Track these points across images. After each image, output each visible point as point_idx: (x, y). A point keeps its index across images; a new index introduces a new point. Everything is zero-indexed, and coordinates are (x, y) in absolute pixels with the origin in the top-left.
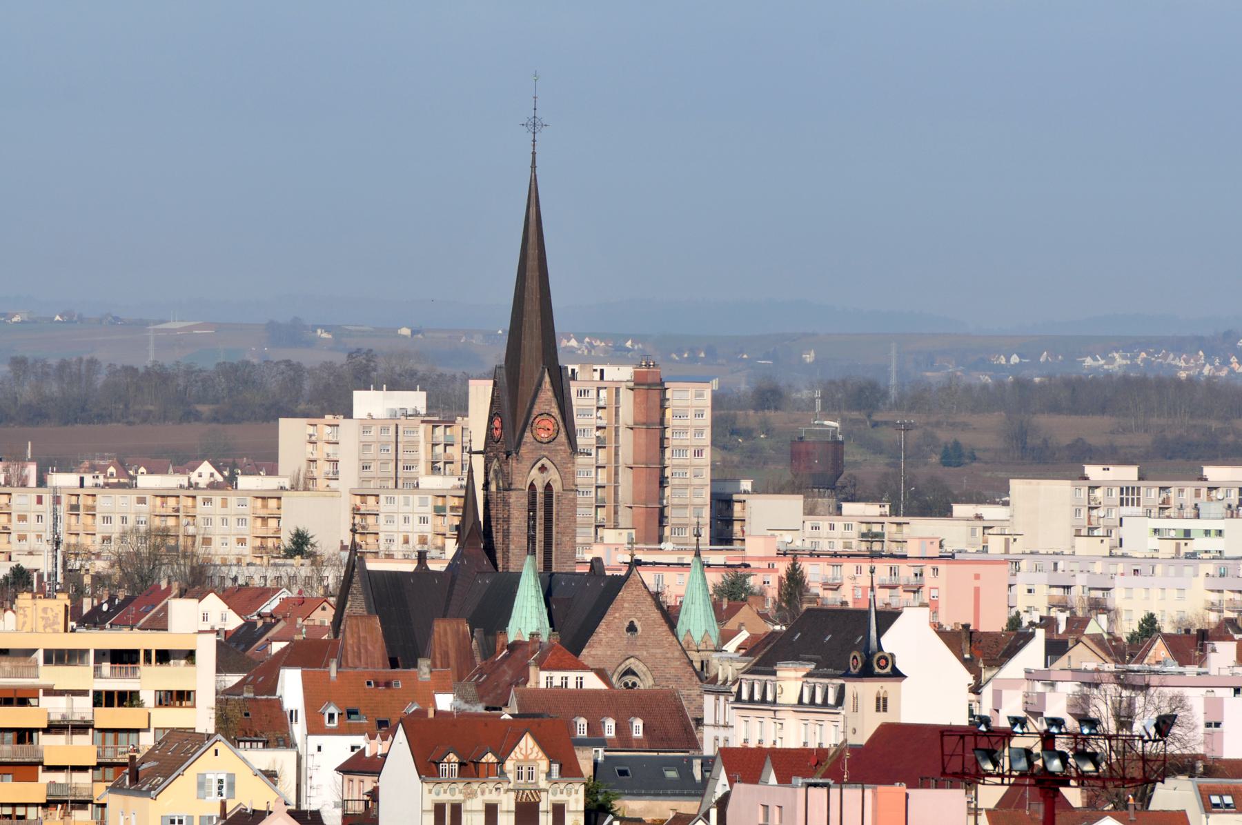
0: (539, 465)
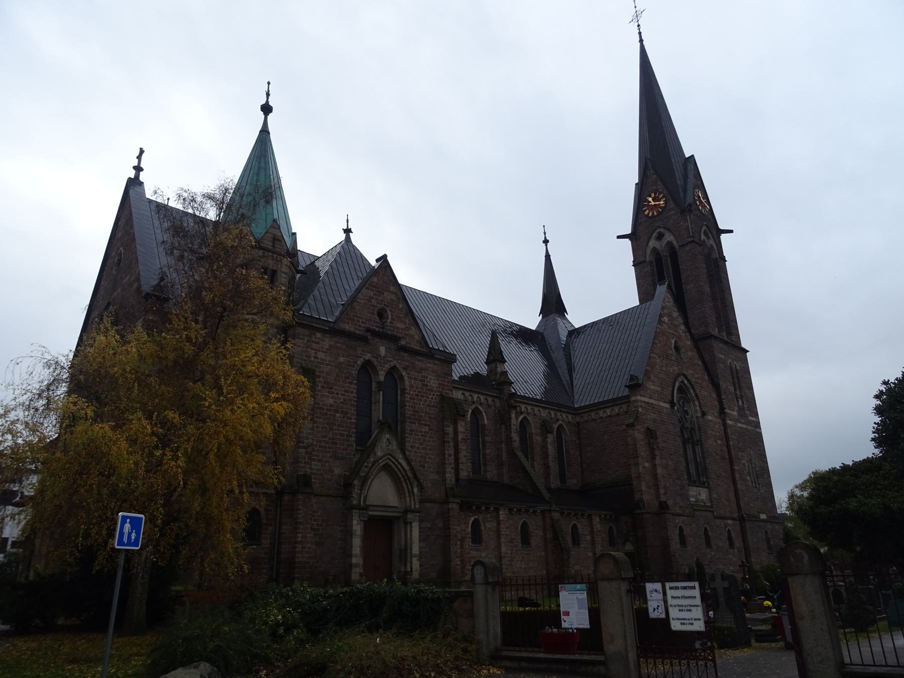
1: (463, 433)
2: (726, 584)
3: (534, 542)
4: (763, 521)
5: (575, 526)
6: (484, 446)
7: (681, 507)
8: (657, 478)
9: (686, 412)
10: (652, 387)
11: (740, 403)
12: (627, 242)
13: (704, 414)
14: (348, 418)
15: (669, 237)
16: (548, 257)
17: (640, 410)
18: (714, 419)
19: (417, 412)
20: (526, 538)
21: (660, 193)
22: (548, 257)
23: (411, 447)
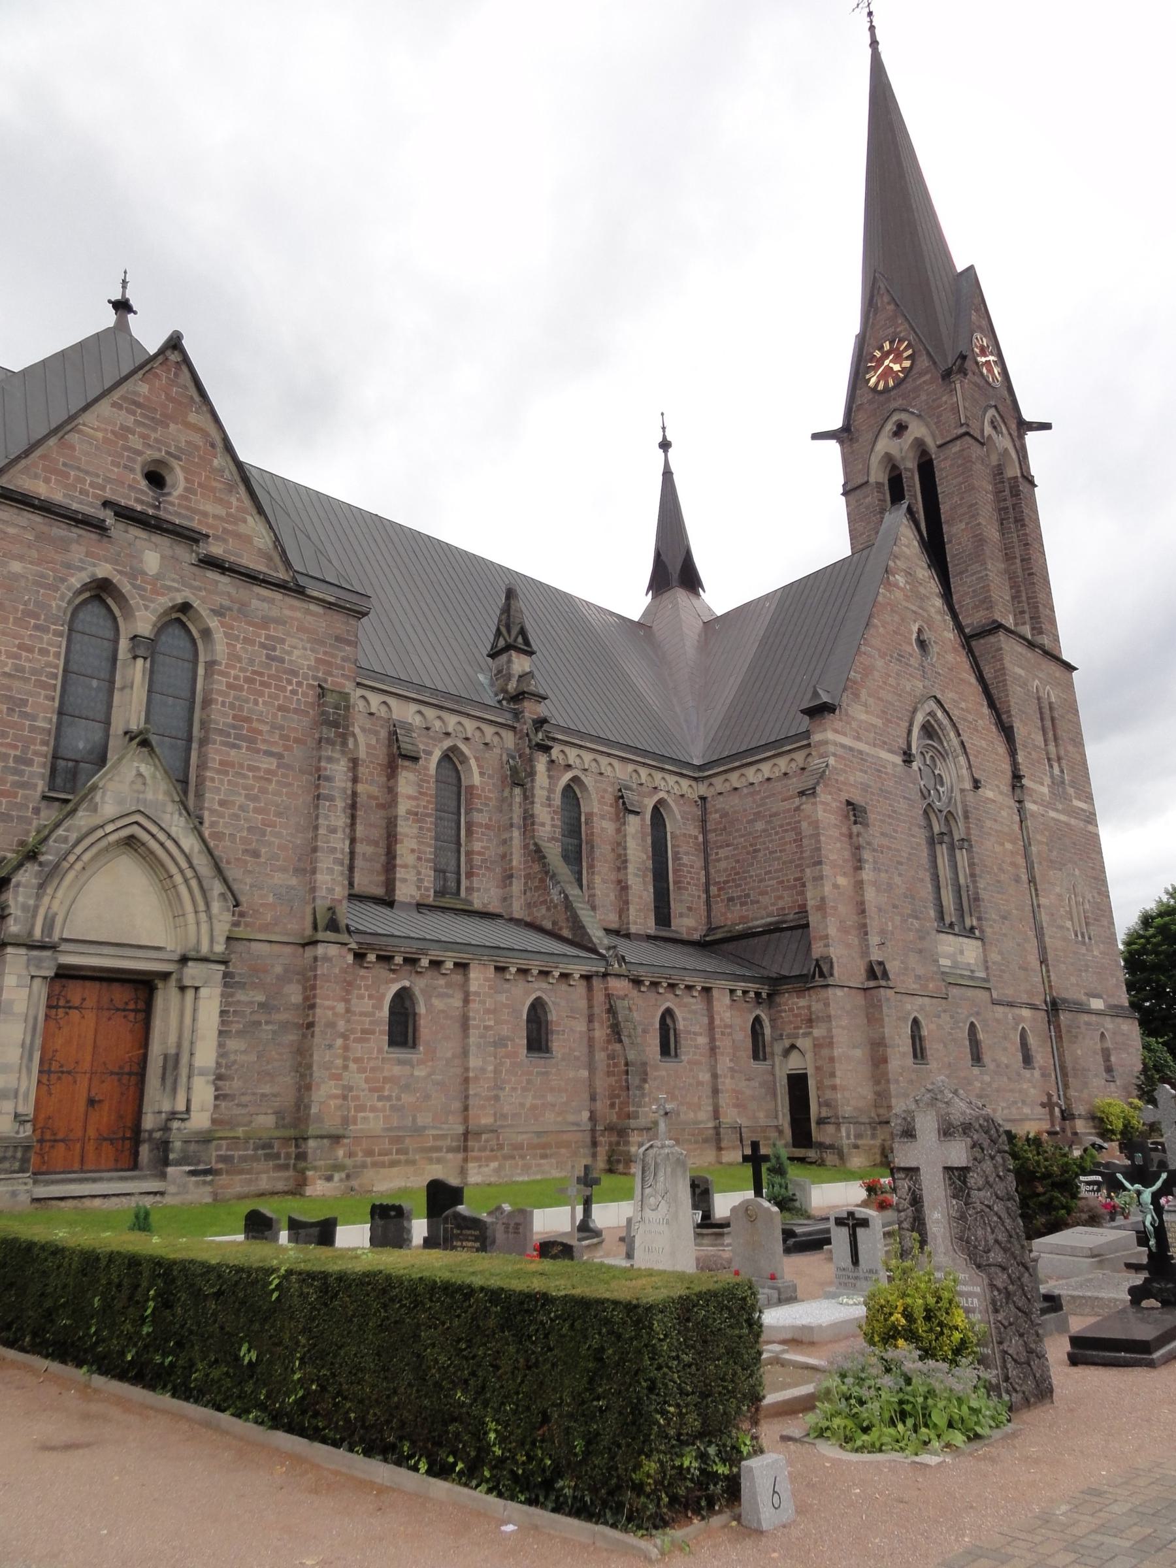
0: (890, 426)
1: (410, 797)
2: (958, 1153)
3: (557, 1045)
4: (1098, 1013)
5: (668, 1012)
6: (469, 832)
7: (919, 977)
8: (863, 911)
9: (940, 779)
10: (863, 717)
11: (1056, 771)
12: (833, 448)
13: (976, 784)
14: (25, 715)
15: (916, 430)
16: (667, 474)
17: (832, 761)
18: (1000, 798)
19: (248, 720)
20: (538, 1038)
21: (901, 341)
22: (667, 474)
23: (222, 803)
